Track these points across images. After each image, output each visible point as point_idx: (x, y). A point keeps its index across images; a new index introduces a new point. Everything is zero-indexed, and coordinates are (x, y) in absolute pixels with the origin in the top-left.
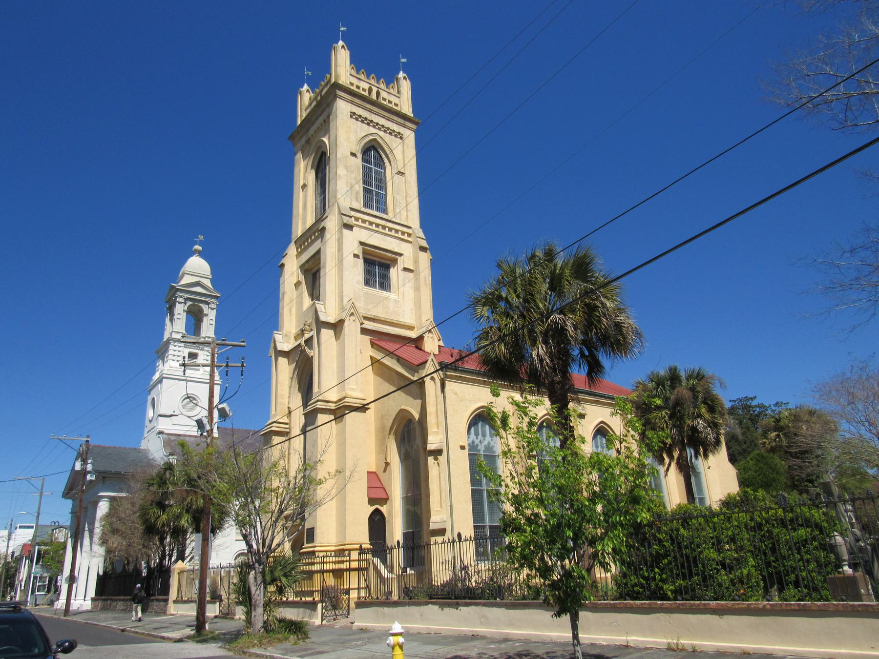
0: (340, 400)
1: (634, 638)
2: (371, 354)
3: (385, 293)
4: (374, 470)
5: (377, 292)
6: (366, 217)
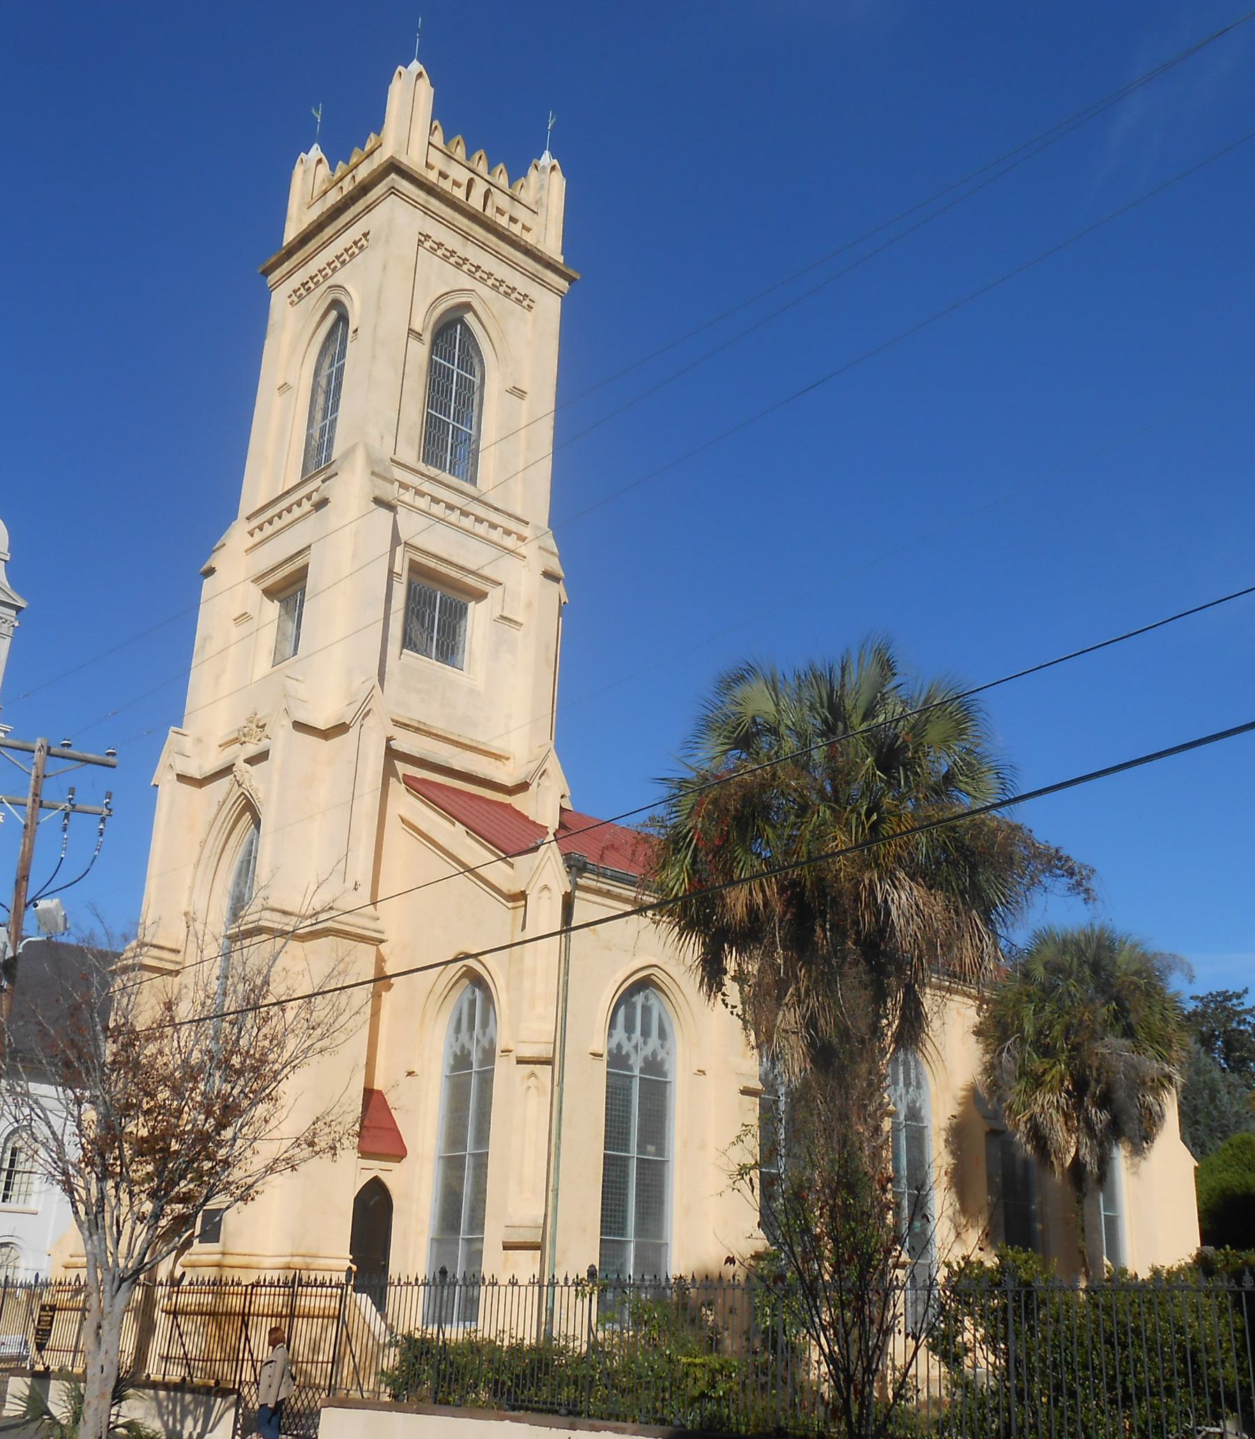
5: (429, 665)
6: (426, 487)
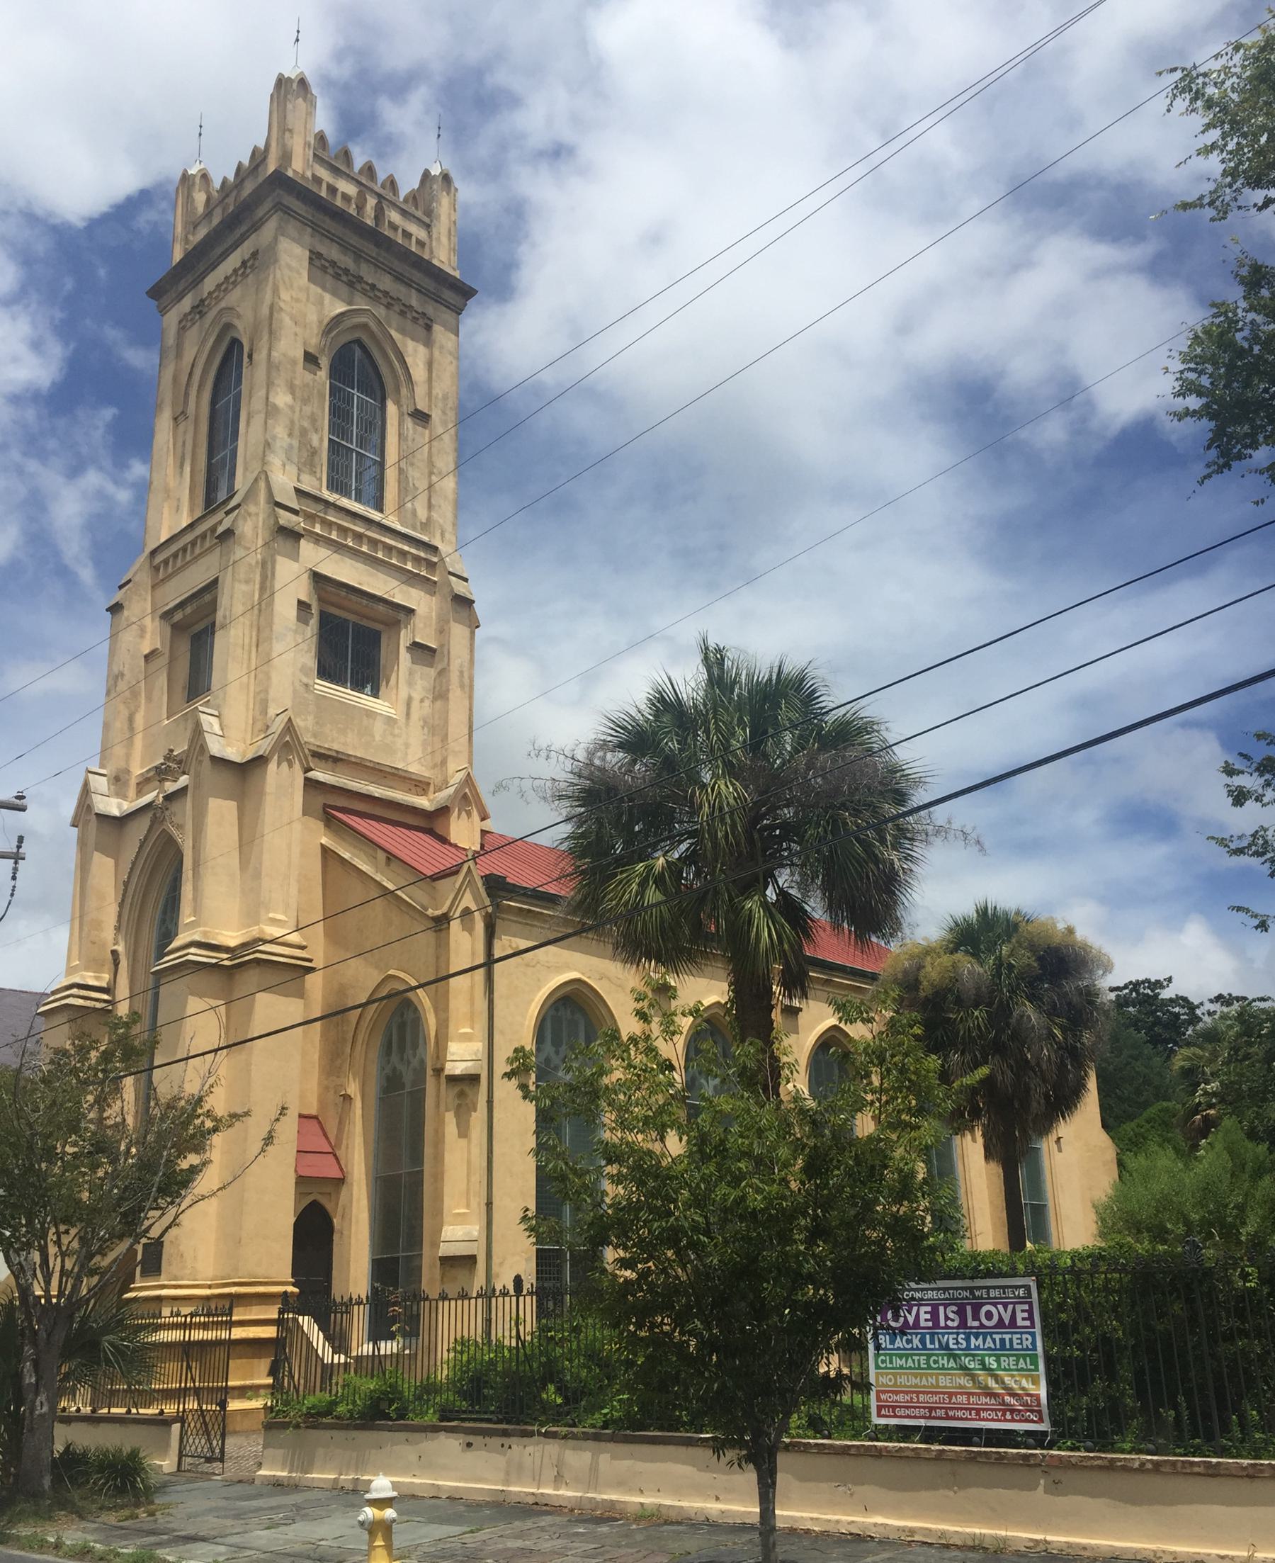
0: (244, 945)
1: (880, 1520)
2: (324, 840)
3: (364, 700)
4: (314, 1112)
